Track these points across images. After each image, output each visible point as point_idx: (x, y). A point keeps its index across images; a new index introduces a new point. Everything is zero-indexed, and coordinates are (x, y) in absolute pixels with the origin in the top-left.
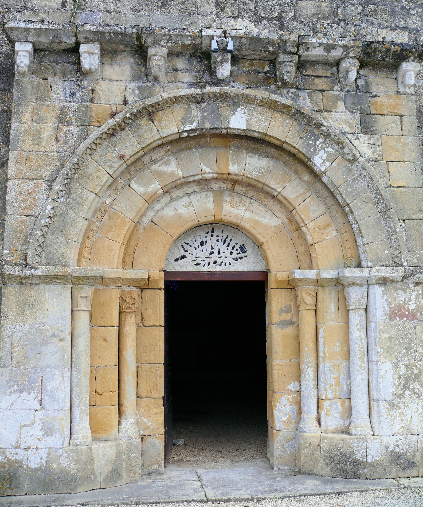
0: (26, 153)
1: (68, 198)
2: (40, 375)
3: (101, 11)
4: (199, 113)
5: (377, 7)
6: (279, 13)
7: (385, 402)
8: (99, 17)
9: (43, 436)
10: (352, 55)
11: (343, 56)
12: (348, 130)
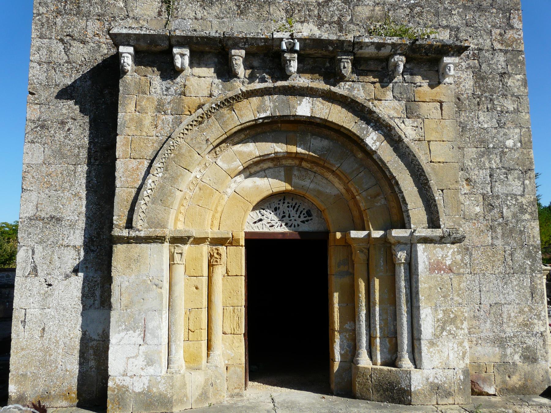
0: (130, 137)
1: (166, 173)
2: (143, 316)
3: (191, 19)
4: (271, 103)
5: (423, 9)
6: (339, 18)
7: (425, 341)
8: (189, 24)
9: (146, 365)
10: (399, 52)
11: (392, 53)
12: (395, 115)
